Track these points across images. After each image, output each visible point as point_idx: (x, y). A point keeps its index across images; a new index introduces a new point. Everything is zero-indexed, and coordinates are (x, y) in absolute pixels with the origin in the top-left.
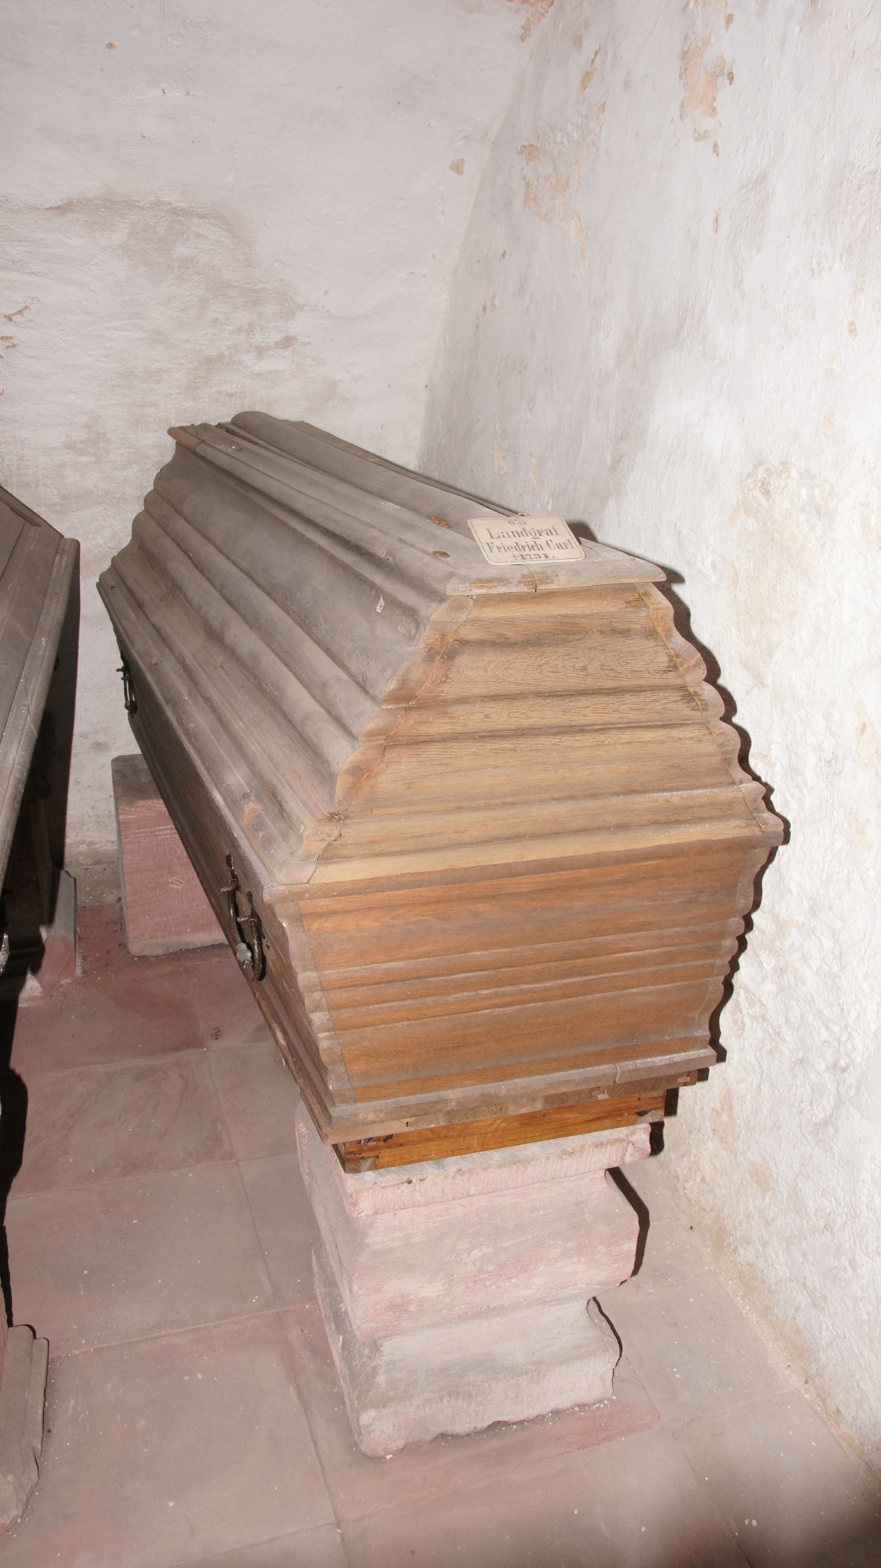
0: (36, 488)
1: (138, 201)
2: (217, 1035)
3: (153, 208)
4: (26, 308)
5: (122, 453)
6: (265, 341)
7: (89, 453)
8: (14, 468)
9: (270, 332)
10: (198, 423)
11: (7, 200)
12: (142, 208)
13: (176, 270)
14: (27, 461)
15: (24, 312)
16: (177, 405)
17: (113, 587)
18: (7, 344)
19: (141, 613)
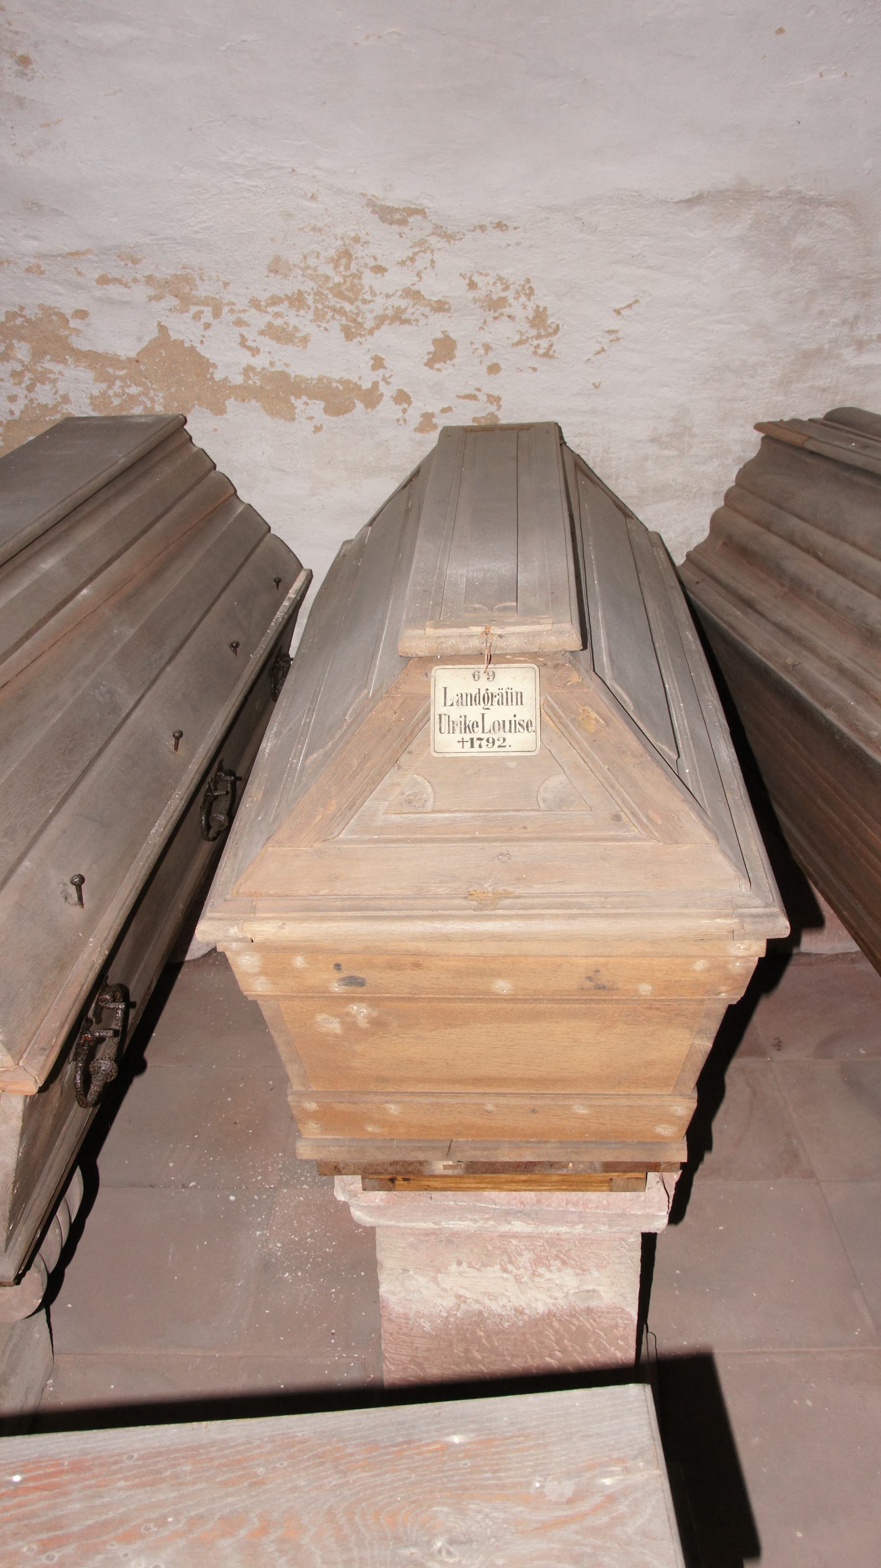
0: (616, 480)
1: (768, 191)
2: (778, 1045)
3: (782, 197)
4: (636, 301)
5: (704, 448)
6: (867, 333)
7: (673, 447)
8: (598, 459)
9: (875, 325)
10: (786, 419)
11: (640, 195)
12: (771, 198)
13: (791, 261)
14: (612, 453)
15: (634, 306)
16: (767, 400)
17: (698, 583)
18: (613, 337)
19: (750, 611)
